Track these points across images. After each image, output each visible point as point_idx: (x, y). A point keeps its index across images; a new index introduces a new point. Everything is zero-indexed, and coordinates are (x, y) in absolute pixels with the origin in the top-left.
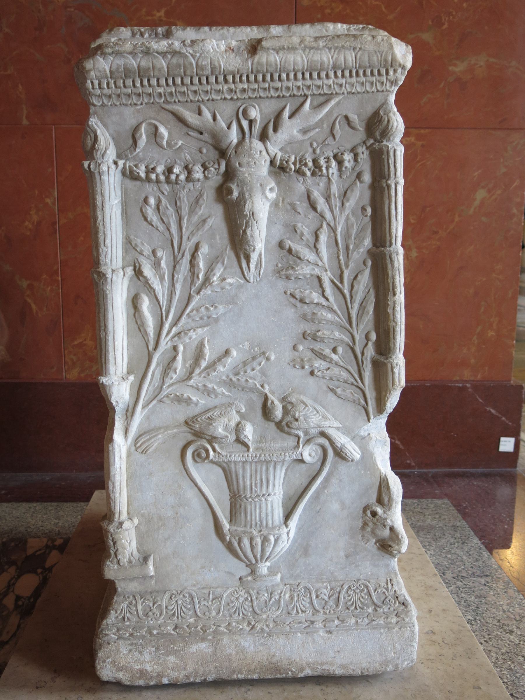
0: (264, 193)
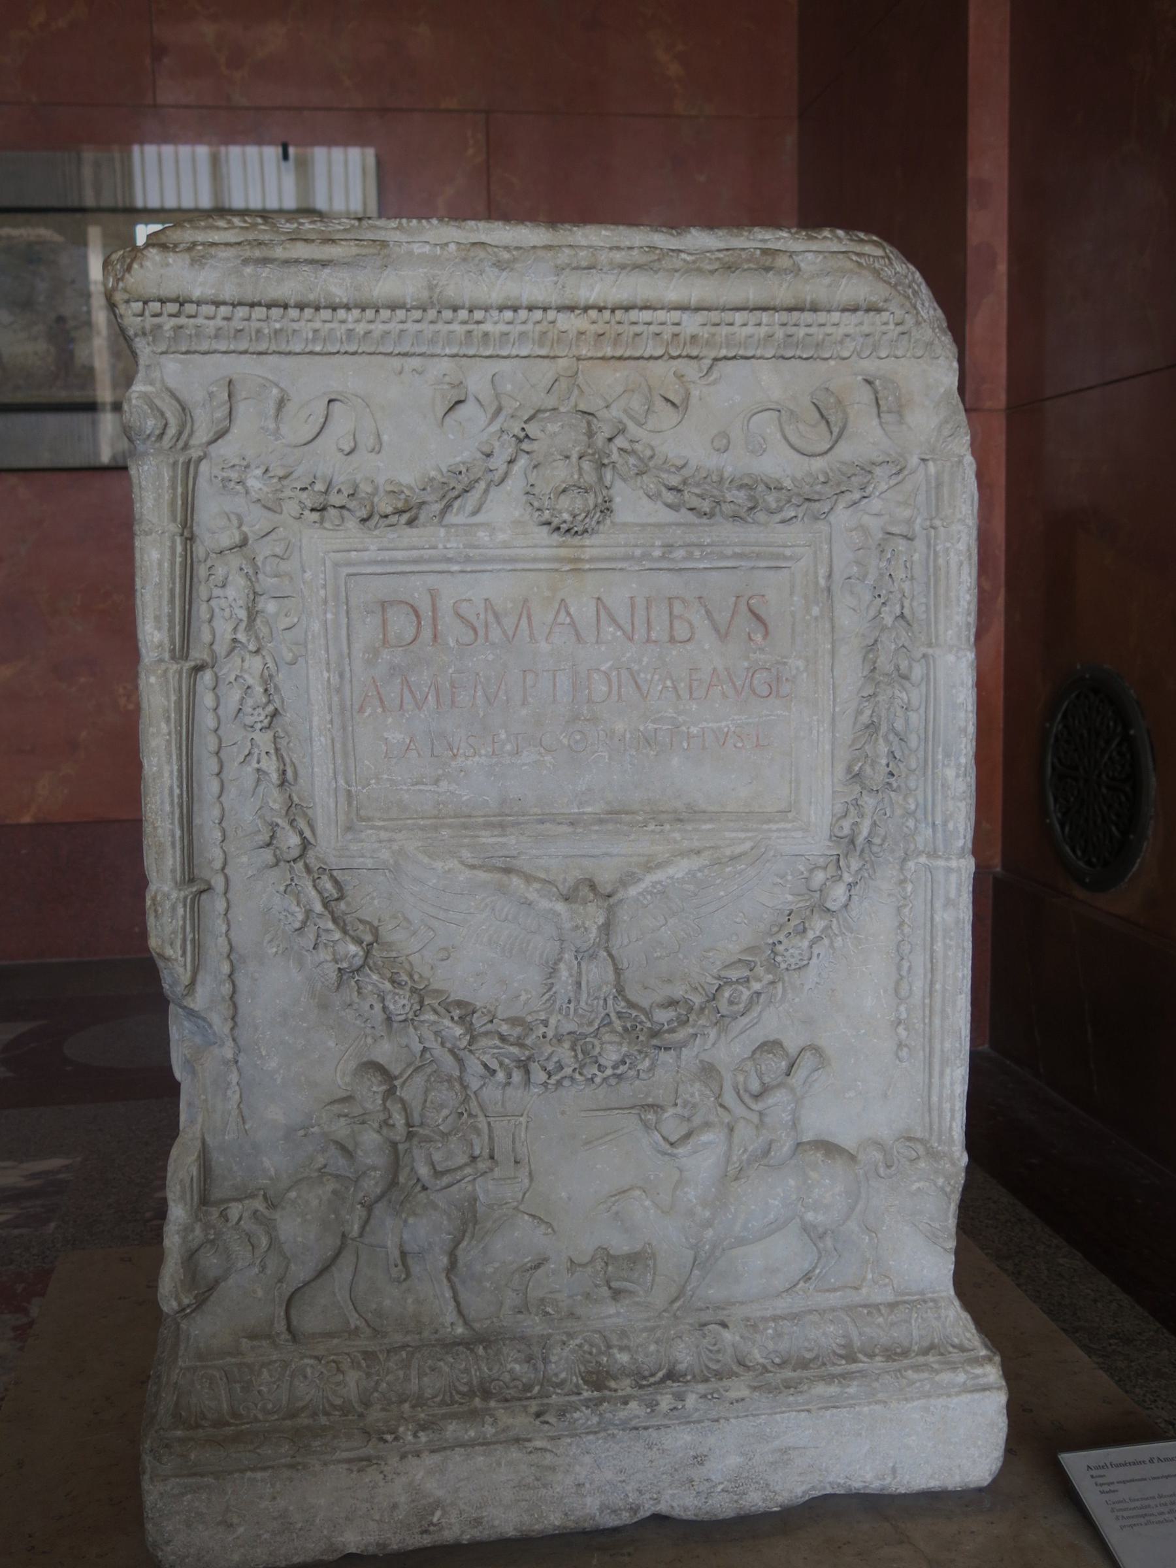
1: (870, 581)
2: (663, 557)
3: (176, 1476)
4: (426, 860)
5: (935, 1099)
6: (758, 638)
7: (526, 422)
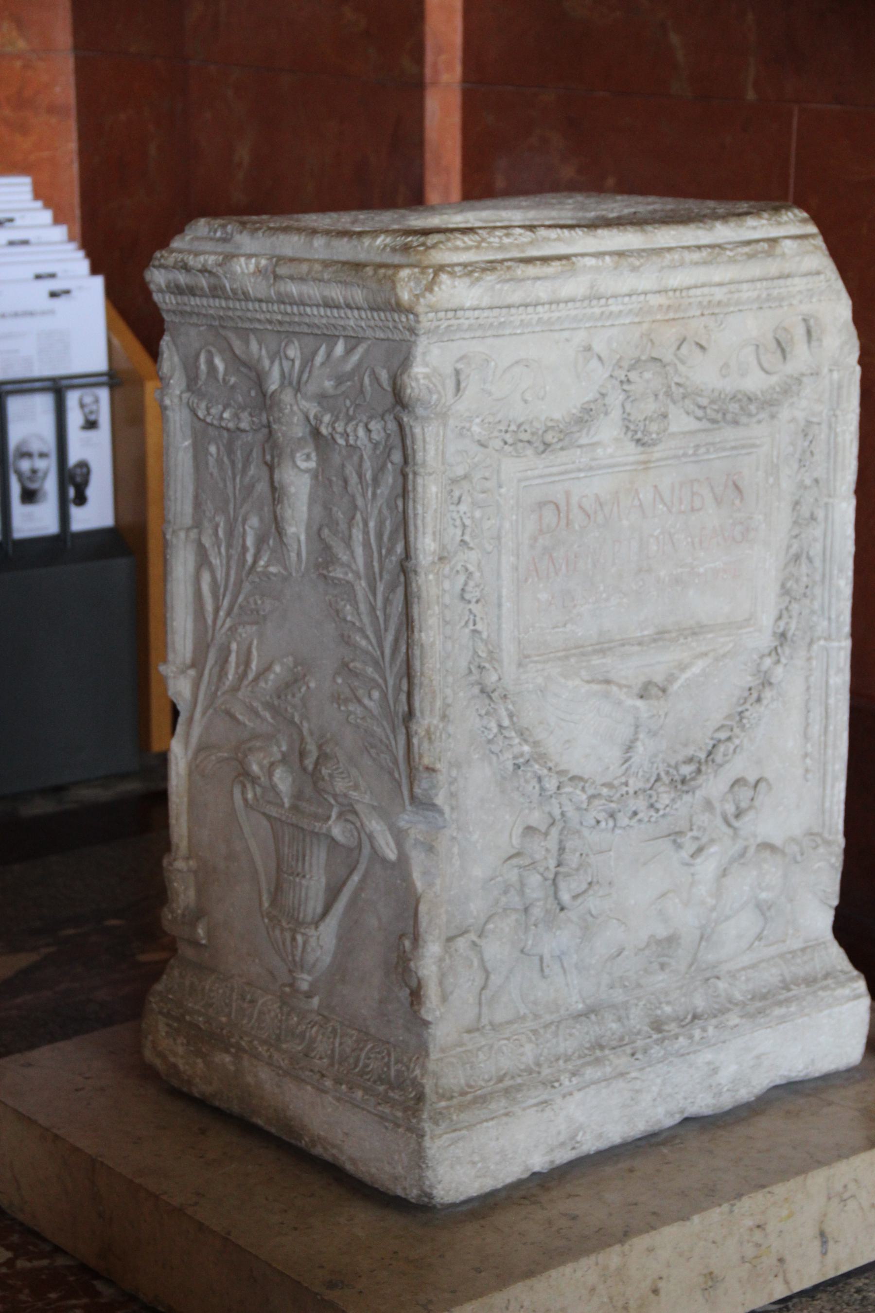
0: (294, 462)
1: (797, 456)
2: (695, 454)
3: (446, 1133)
4: (563, 681)
5: (827, 805)
6: (737, 502)
7: (628, 371)
